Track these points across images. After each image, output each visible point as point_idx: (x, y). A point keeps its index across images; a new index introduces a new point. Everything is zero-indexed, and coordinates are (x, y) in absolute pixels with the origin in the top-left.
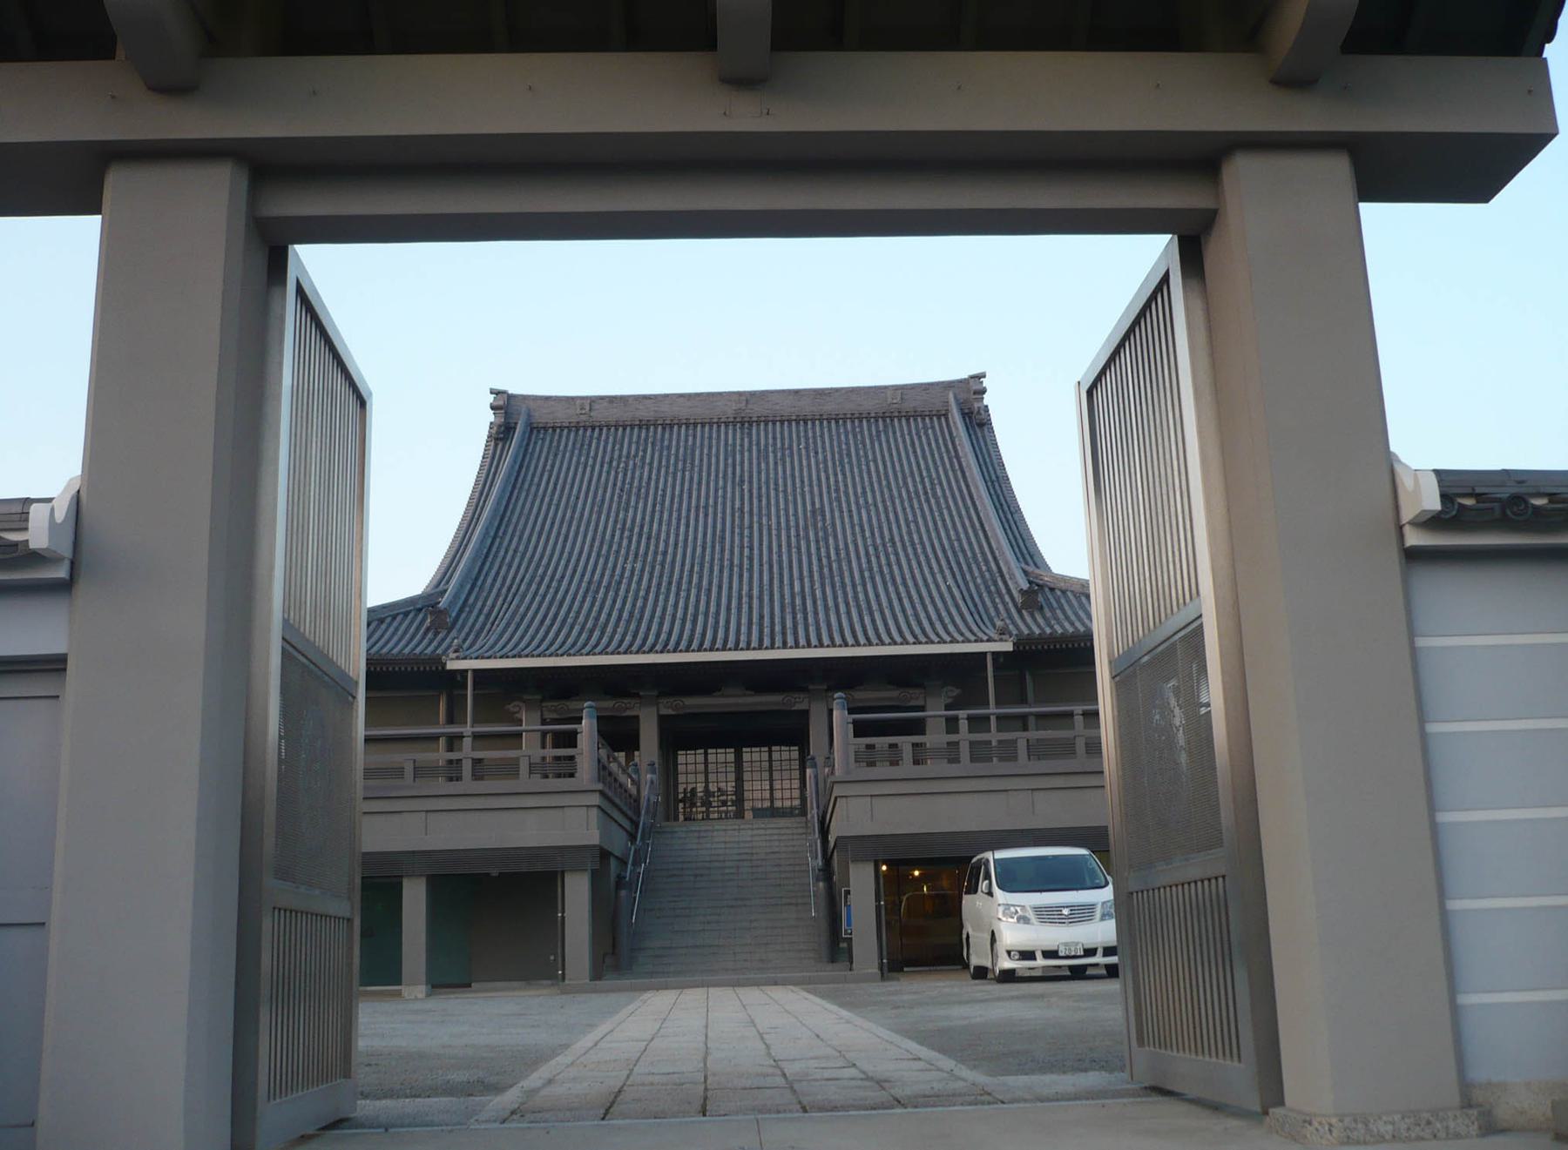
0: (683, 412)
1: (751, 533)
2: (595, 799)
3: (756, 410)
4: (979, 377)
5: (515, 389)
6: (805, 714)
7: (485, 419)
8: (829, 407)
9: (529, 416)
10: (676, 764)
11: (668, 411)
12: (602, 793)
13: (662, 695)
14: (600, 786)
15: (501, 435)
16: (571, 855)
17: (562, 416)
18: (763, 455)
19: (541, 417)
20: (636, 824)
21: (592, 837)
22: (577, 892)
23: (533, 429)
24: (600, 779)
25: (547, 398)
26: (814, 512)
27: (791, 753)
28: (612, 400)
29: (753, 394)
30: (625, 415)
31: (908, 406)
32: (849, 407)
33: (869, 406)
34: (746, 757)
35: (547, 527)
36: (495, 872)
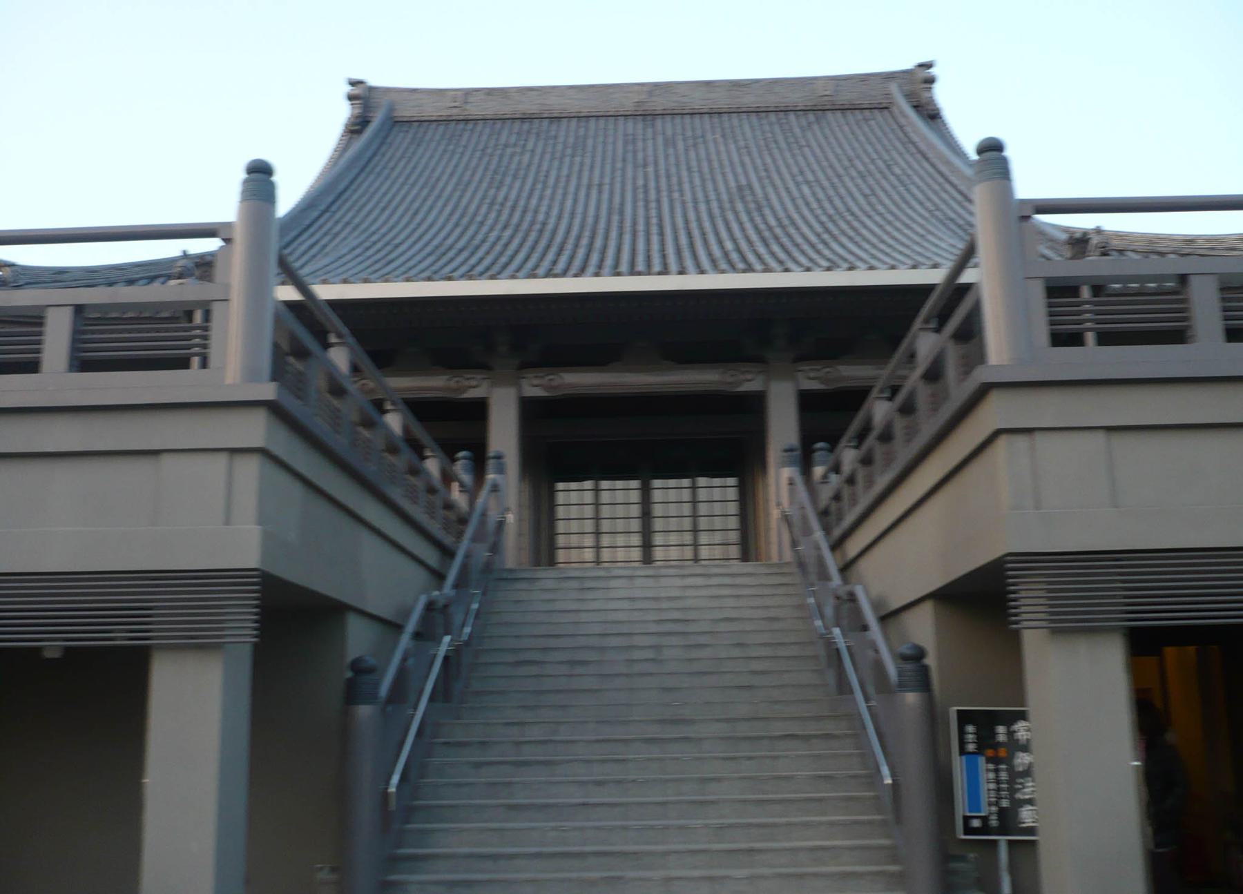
0: (574, 106)
1: (659, 208)
2: (254, 430)
3: (659, 104)
4: (928, 65)
5: (374, 80)
6: (754, 405)
7: (343, 112)
8: (749, 100)
9: (391, 109)
10: (552, 506)
11: (556, 105)
12: (272, 407)
13: (526, 366)
14: (268, 391)
15: (356, 127)
16: (174, 600)
17: (431, 110)
18: (670, 142)
19: (406, 111)
20: (447, 553)
21: (241, 547)
22: (192, 716)
23: (395, 123)
24: (278, 373)
25: (414, 91)
26: (740, 188)
27: (719, 493)
28: (490, 92)
29: (657, 86)
30: (506, 109)
31: (844, 98)
32: (771, 100)
33: (796, 98)
34: (657, 495)
35: (394, 203)
36: (52, 648)
